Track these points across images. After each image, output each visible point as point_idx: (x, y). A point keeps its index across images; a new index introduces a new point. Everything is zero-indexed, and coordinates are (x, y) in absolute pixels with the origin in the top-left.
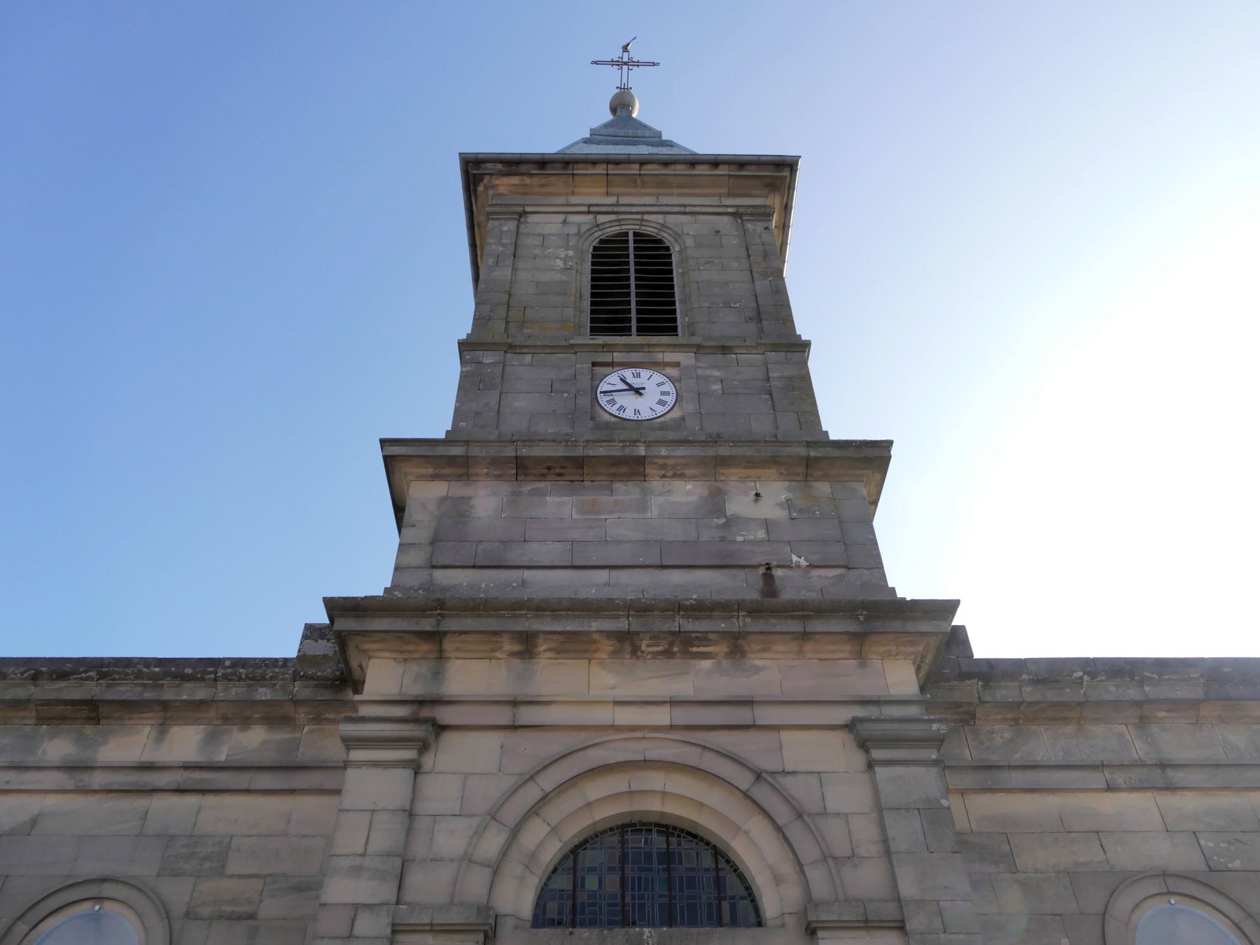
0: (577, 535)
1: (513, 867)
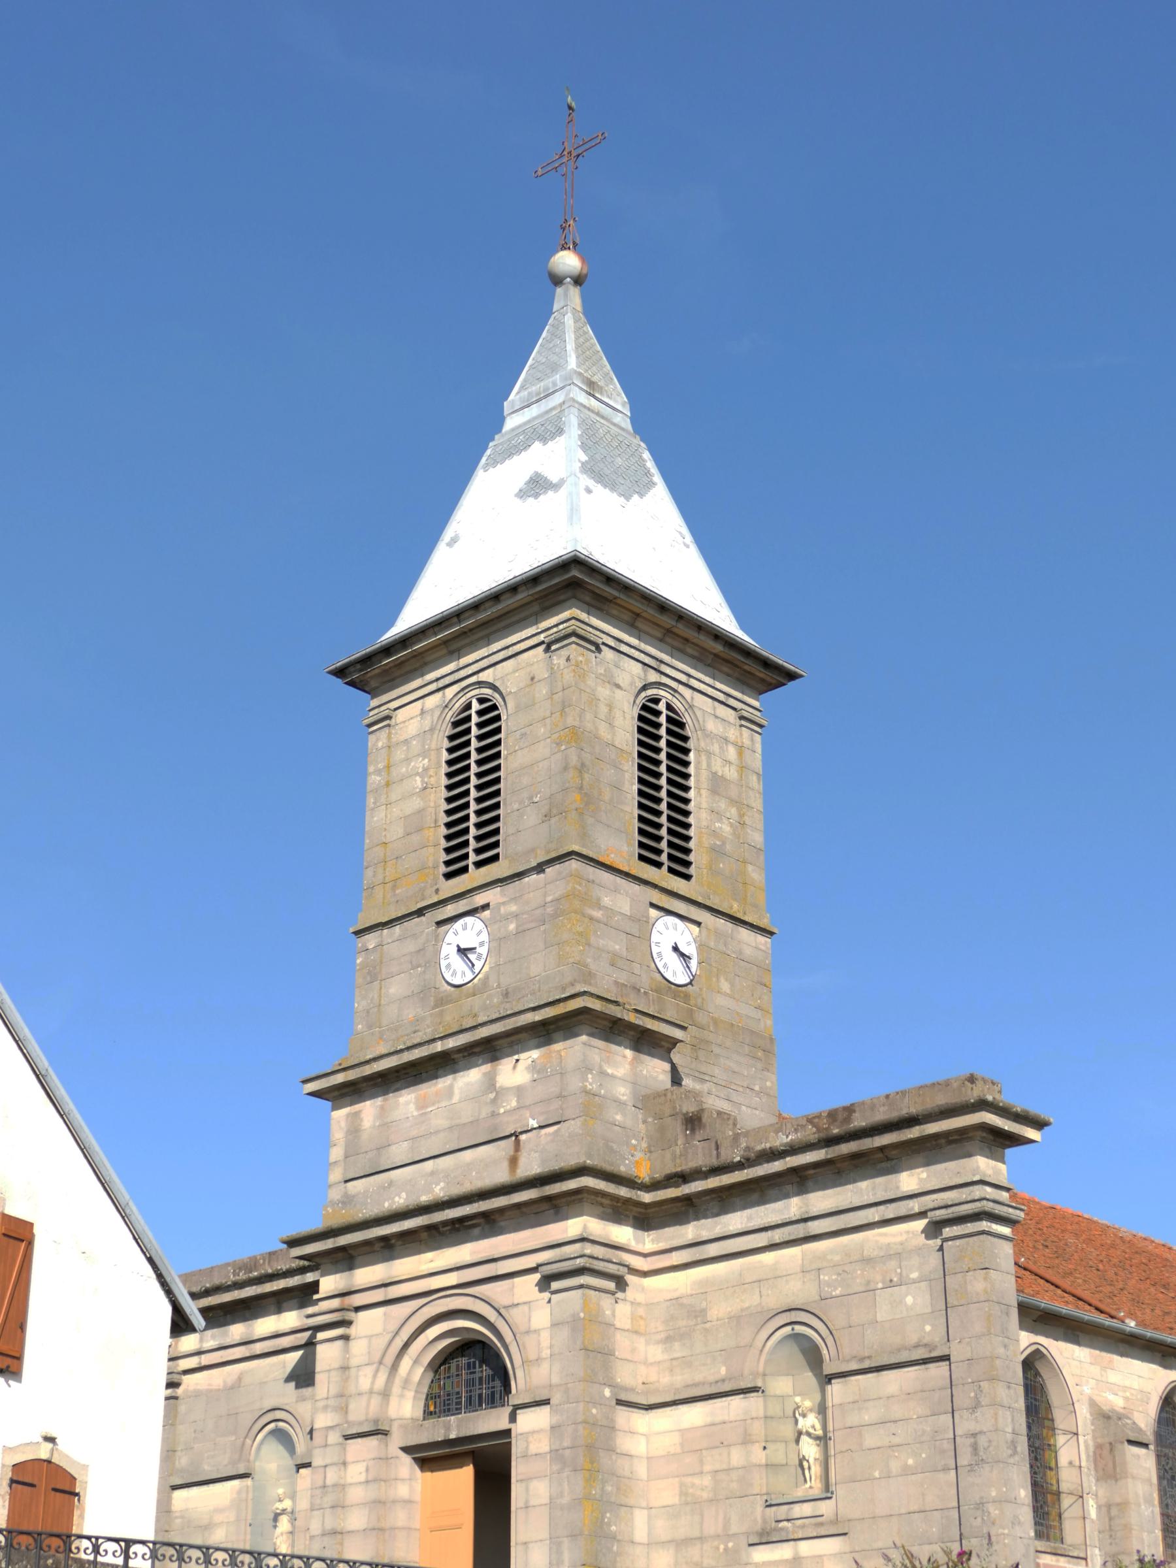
0: (414, 1133)
1: (396, 1389)
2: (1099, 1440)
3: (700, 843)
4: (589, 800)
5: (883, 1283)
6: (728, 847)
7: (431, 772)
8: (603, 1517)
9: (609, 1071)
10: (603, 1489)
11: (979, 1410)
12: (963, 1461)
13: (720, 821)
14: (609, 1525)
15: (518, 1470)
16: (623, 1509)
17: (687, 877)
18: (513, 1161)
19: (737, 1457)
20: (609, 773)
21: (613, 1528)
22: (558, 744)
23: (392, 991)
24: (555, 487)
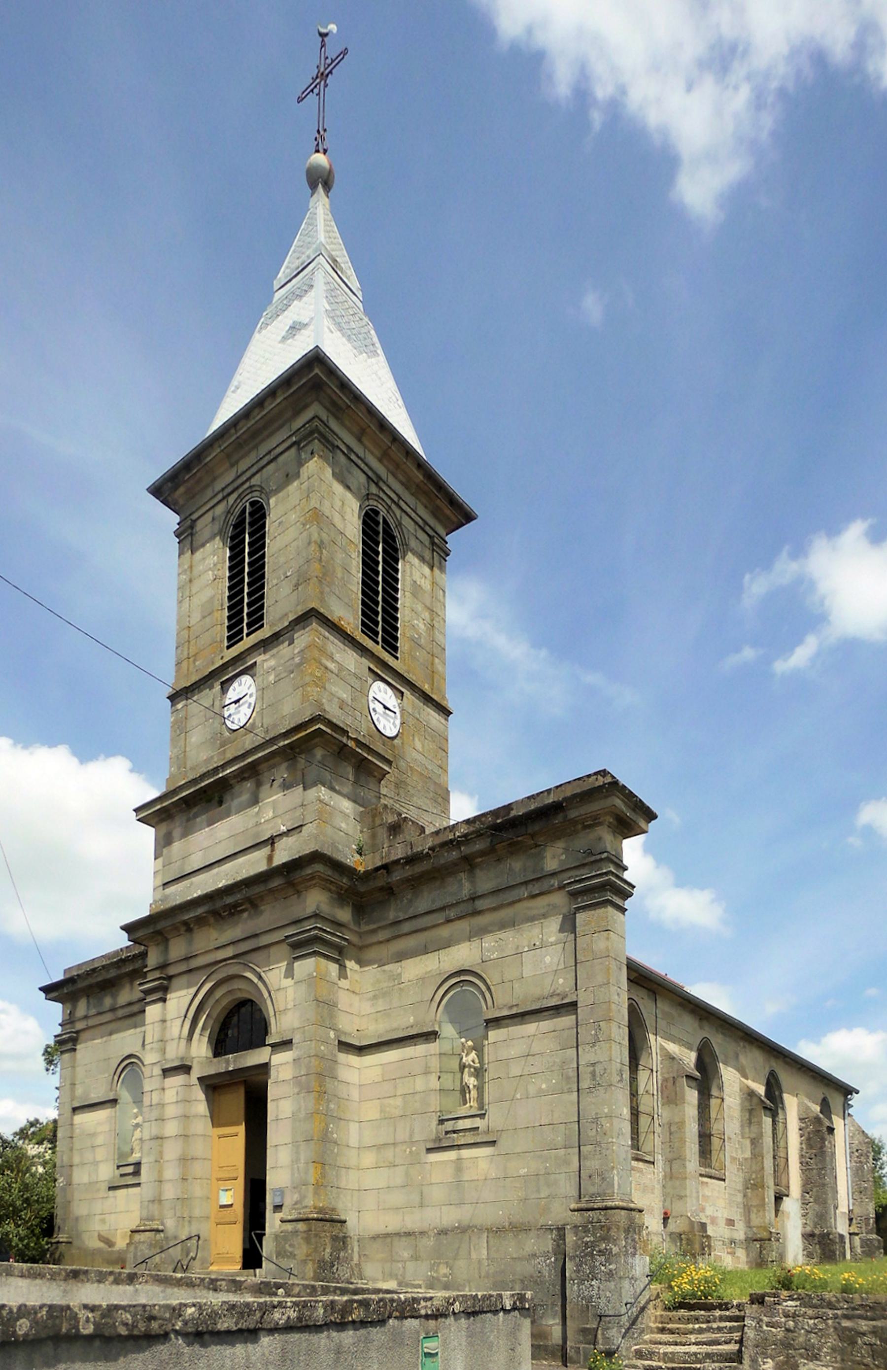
2: (666, 1076)
3: (404, 634)
4: (325, 576)
5: (528, 947)
6: (423, 640)
7: (219, 566)
8: (327, 1125)
9: (337, 788)
10: (327, 1106)
11: (598, 1044)
12: (584, 1085)
13: (417, 620)
14: (332, 1133)
15: (272, 1092)
16: (342, 1122)
17: (397, 658)
18: (270, 858)
19: (420, 1084)
20: (339, 556)
21: (335, 1136)
22: (304, 525)
23: (193, 740)
24: (306, 325)
